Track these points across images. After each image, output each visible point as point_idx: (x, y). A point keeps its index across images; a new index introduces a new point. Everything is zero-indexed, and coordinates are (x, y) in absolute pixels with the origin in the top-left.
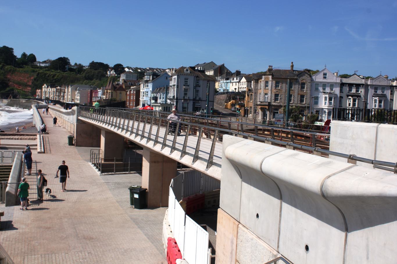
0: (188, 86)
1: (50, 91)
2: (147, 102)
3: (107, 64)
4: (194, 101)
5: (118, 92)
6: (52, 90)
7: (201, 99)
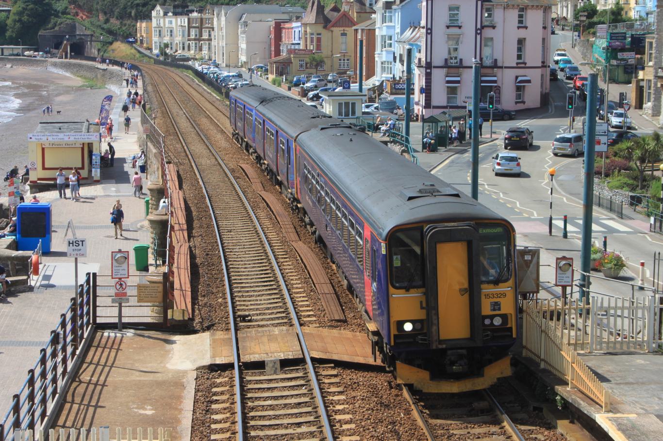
0: (460, 27)
1: (174, 25)
2: (390, 66)
5: (337, 31)
6: (179, 23)
7: (499, 64)
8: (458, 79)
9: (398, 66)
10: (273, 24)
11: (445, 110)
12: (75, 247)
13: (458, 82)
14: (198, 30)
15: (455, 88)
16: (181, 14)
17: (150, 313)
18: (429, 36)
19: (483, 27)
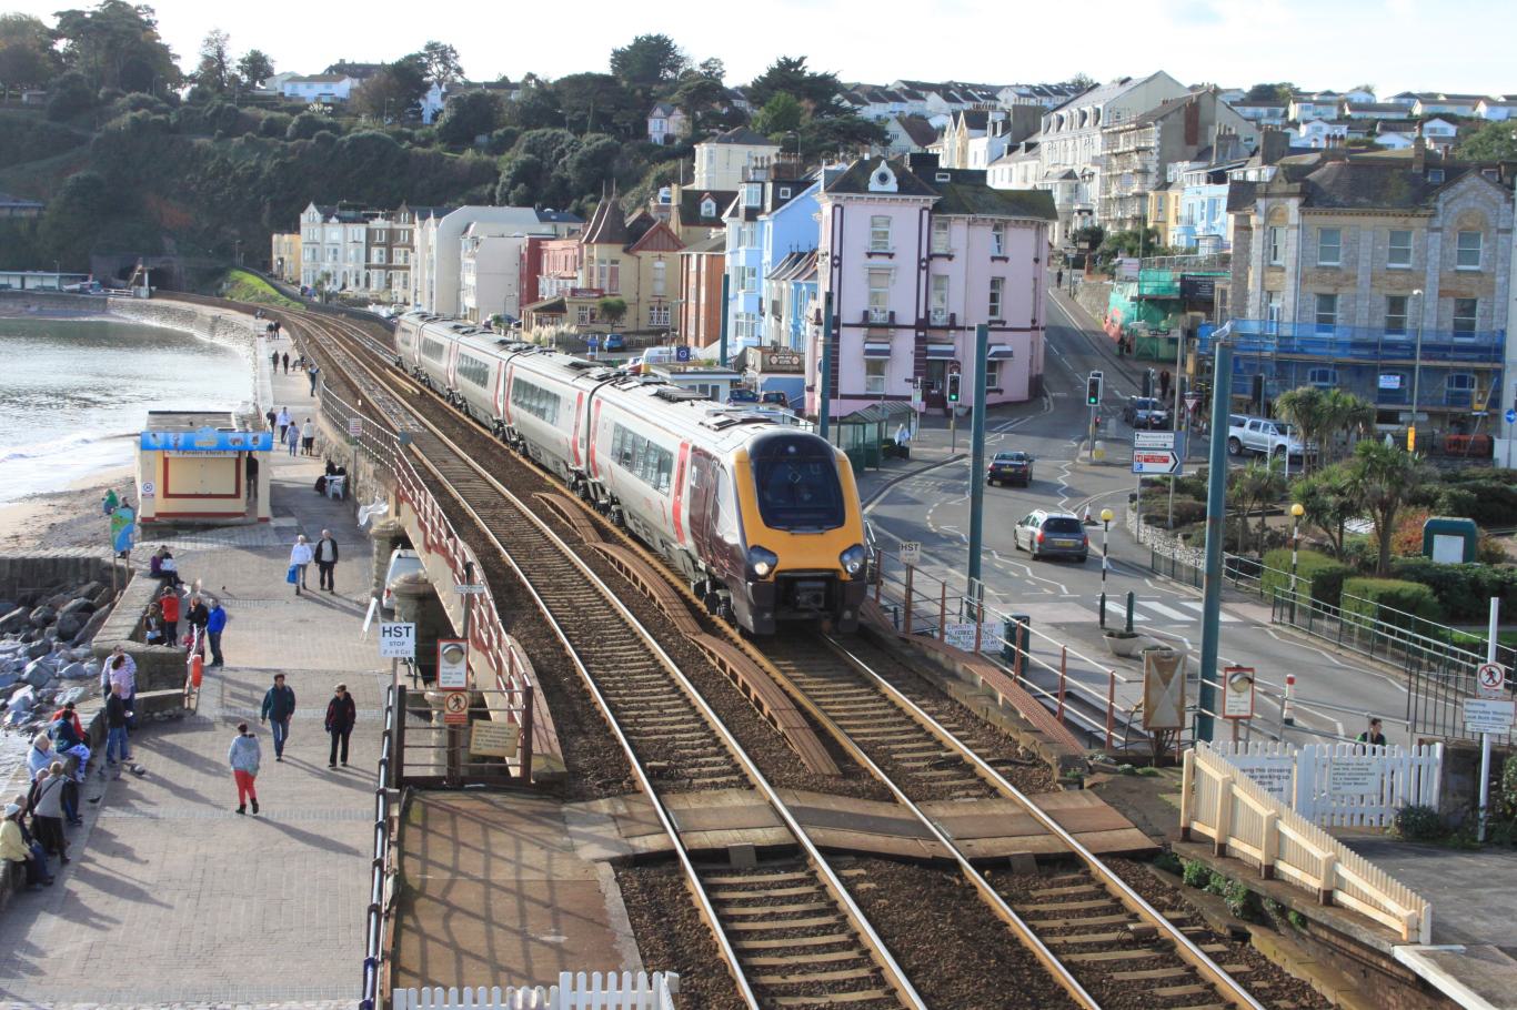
0: (891, 256)
3: (831, 73)
4: (921, 334)
7: (959, 323)
8: (886, 347)
9: (769, 320)
10: (525, 242)
11: (876, 402)
12: (394, 639)
13: (887, 353)
14: (384, 249)
15: (881, 363)
16: (354, 221)
17: (433, 760)
18: (836, 271)
19: (931, 257)
